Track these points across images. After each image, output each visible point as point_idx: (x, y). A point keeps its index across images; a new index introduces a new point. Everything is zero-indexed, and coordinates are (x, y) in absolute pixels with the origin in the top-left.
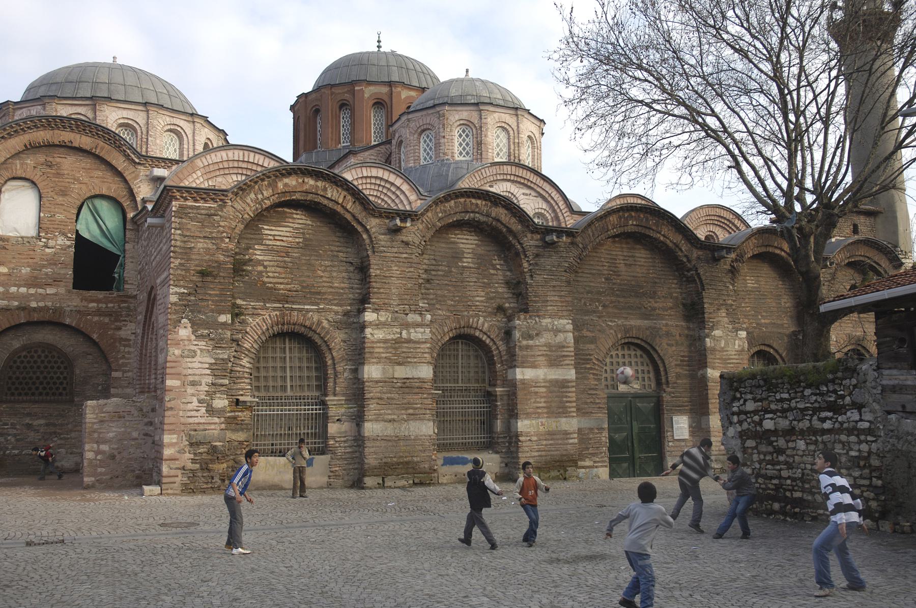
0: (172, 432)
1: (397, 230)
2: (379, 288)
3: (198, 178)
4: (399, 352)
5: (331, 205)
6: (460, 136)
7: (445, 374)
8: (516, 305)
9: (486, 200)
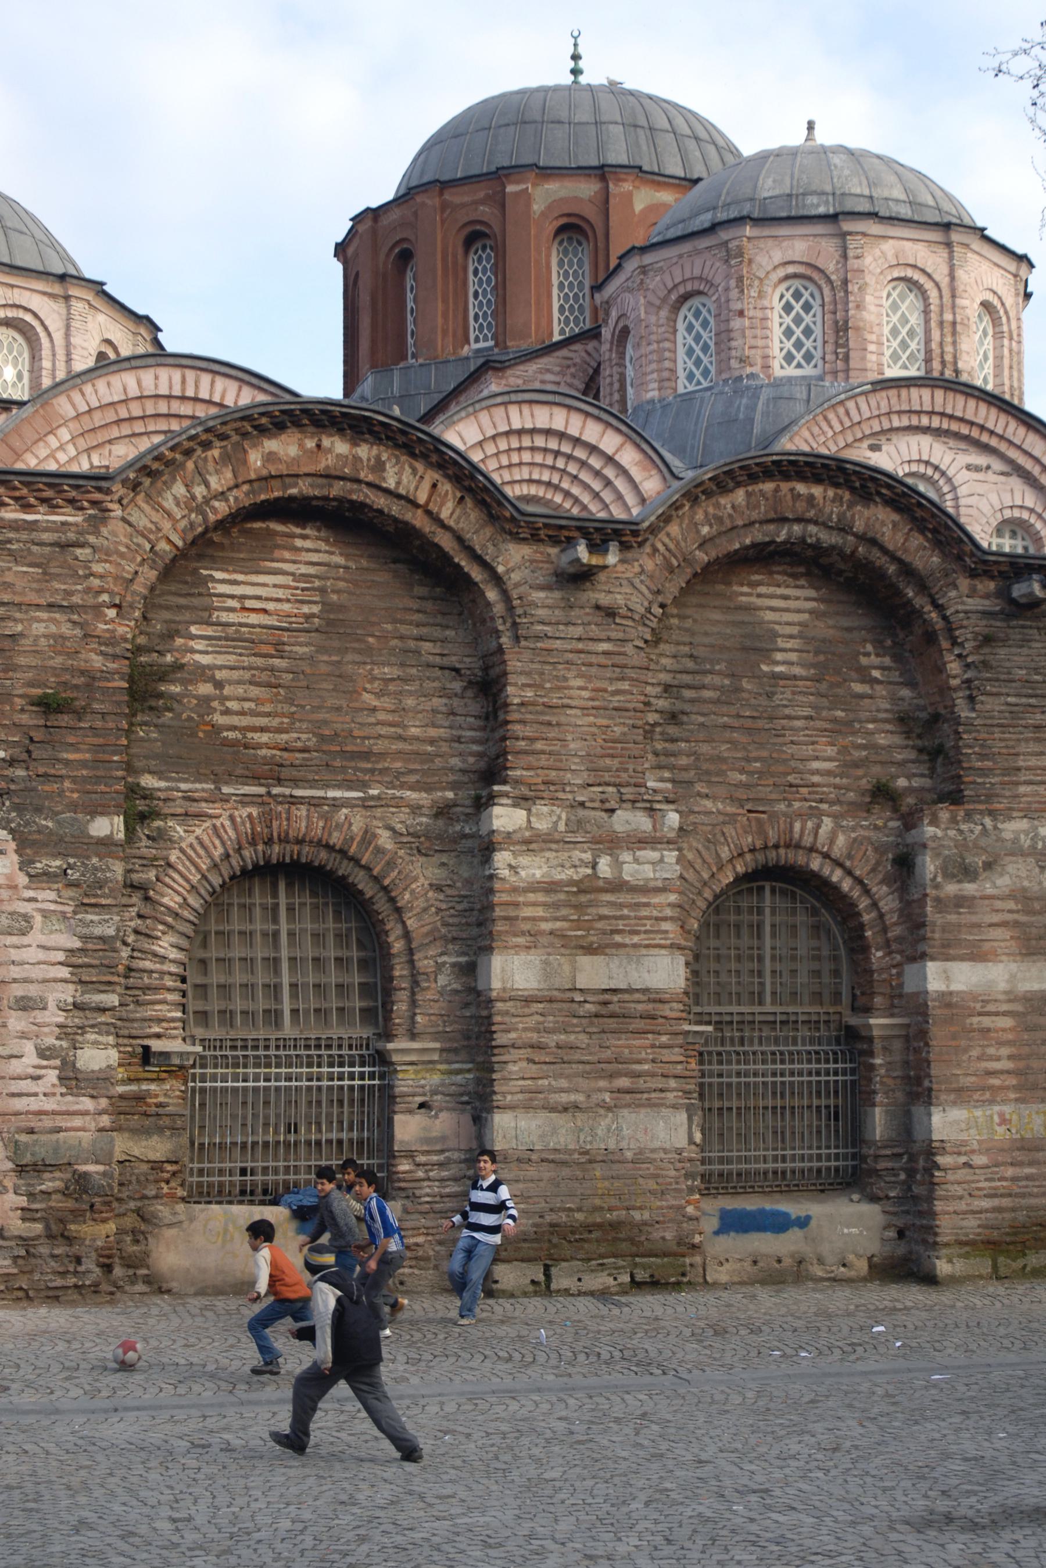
1: (581, 577)
2: (532, 740)
3: (61, 448)
4: (589, 916)
5: (395, 509)
6: (788, 308)
7: (724, 978)
8: (926, 782)
9: (837, 485)
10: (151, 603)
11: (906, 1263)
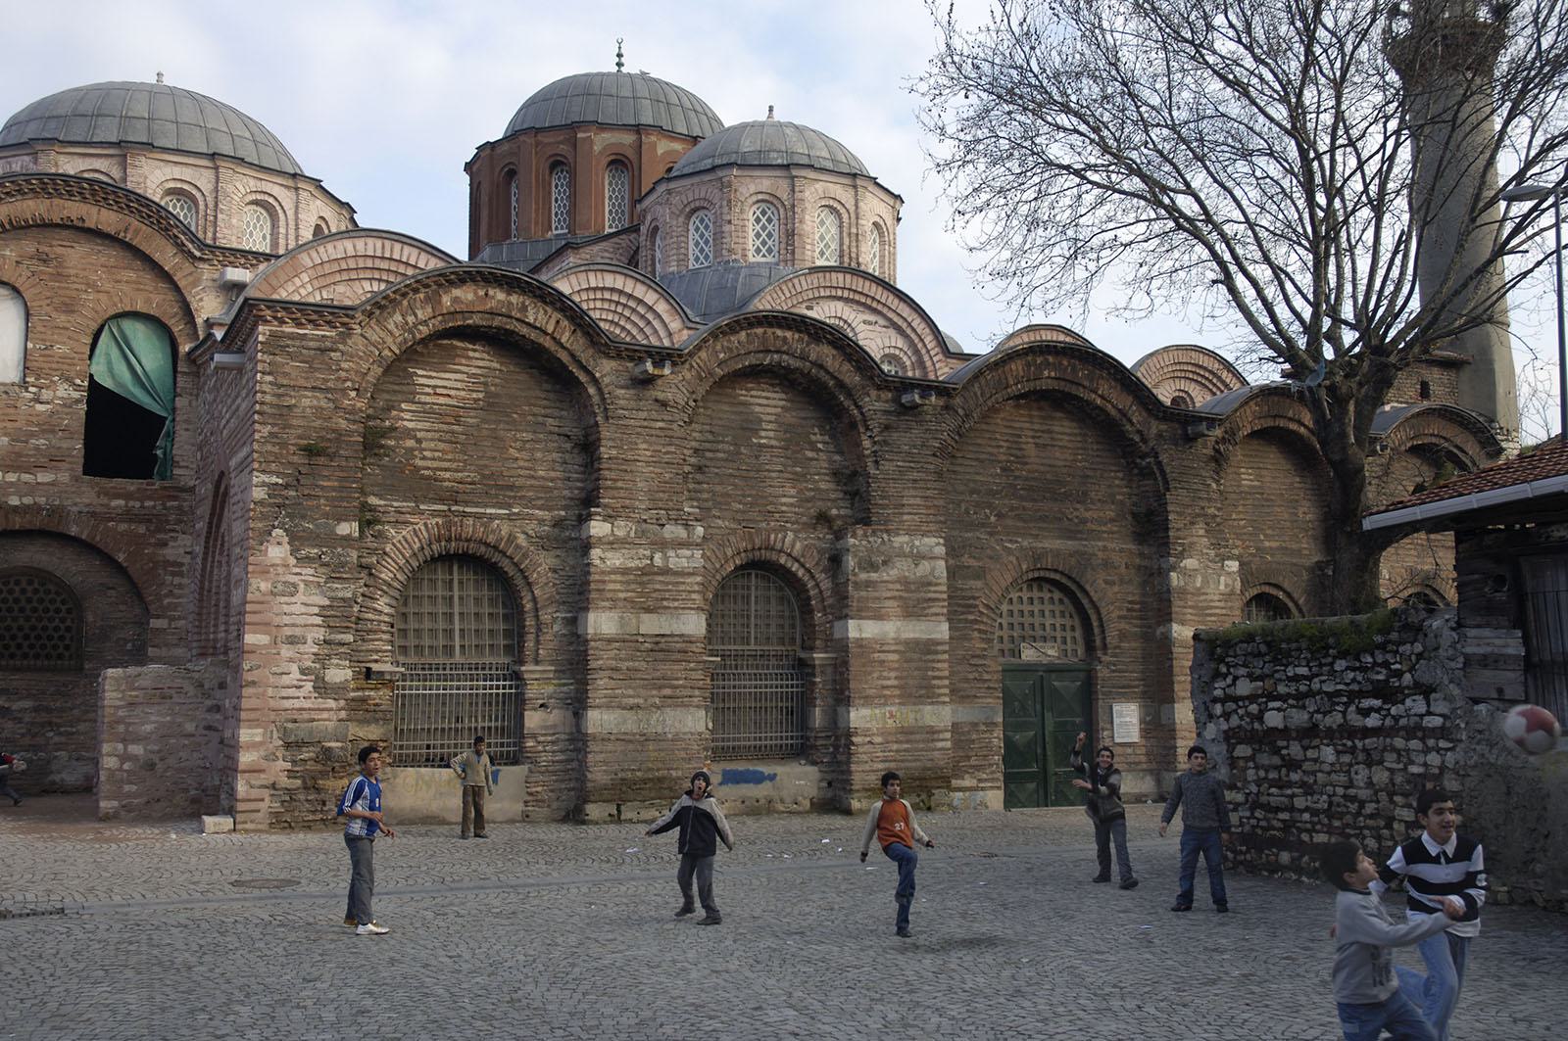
0: (254, 723)
3: (303, 286)
4: (649, 589)
5: (533, 335)
6: (758, 220)
8: (848, 512)
9: (800, 332)
10: (377, 389)
11: (833, 802)
